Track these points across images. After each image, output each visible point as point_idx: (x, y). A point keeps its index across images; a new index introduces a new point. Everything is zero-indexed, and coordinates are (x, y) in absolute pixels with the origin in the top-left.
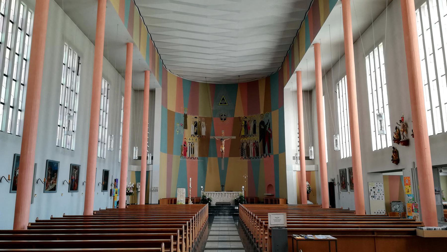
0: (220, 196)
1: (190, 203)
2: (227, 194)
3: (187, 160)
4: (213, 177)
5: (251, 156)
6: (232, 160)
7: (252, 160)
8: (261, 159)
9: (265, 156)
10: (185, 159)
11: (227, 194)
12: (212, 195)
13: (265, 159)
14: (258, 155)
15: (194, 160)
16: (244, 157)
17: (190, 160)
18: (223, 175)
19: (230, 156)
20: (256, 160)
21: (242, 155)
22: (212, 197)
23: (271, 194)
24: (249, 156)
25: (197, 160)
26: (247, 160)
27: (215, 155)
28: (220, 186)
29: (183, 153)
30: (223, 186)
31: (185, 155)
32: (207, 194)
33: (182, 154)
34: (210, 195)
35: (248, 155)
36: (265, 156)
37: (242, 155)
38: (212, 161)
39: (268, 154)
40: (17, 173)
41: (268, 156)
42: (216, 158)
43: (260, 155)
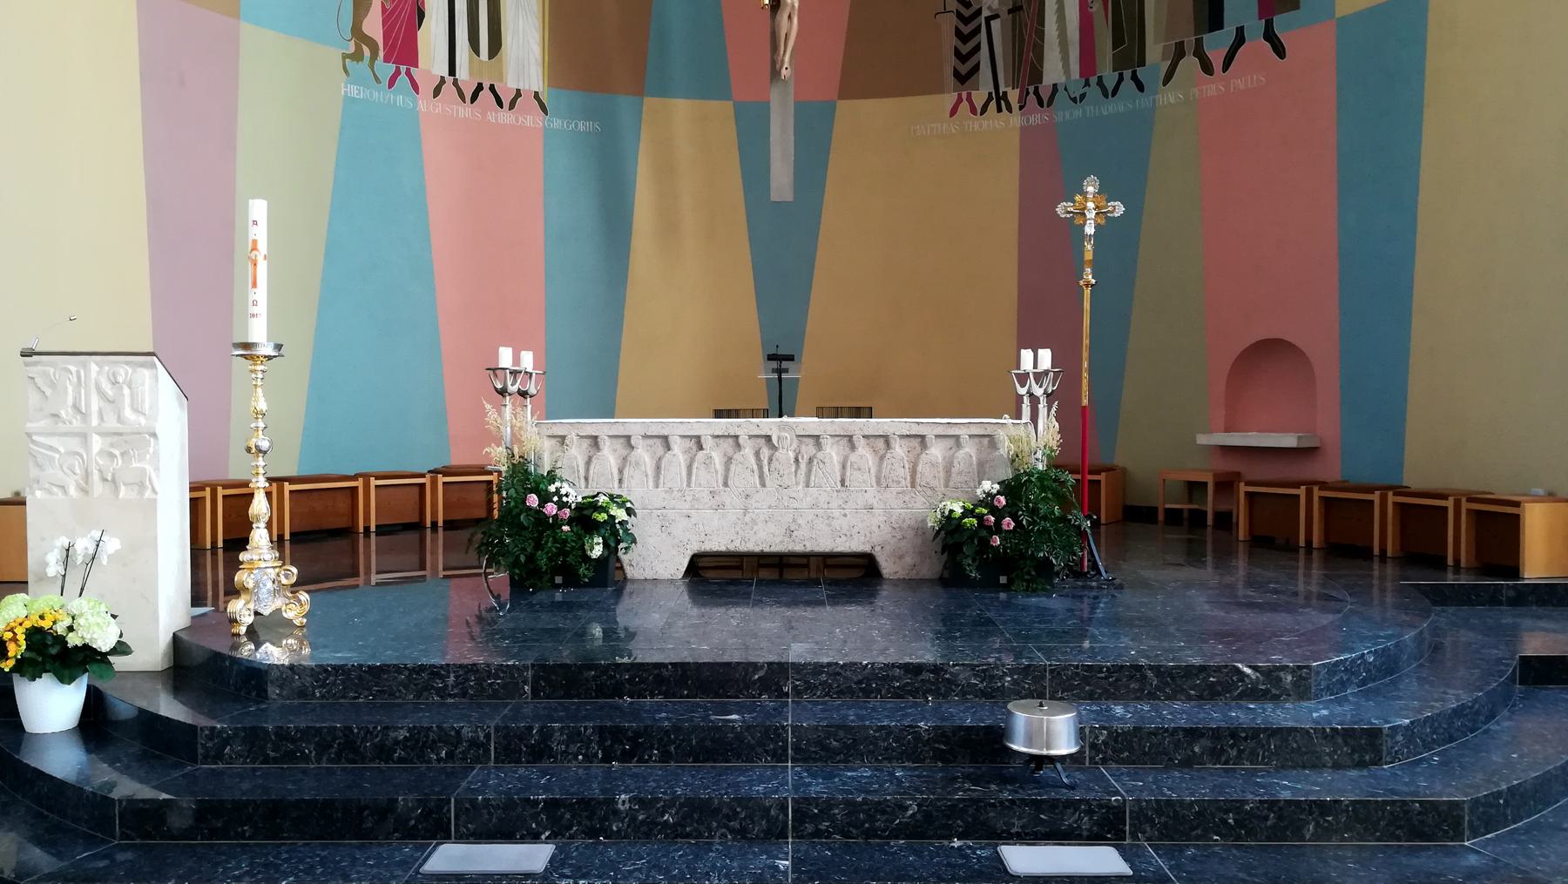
0: (744, 476)
1: (263, 565)
2: (832, 453)
3: (424, 103)
4: (688, 289)
5: (1053, 72)
6: (865, 121)
7: (1064, 113)
8: (1168, 97)
9: (1216, 56)
10: (400, 96)
11: (832, 453)
12: (644, 455)
13: (1213, 87)
14: (1130, 52)
15: (505, 116)
16: (979, 97)
17: (466, 111)
18: (782, 250)
19: (841, 97)
20: (1113, 107)
21: (964, 78)
22: (636, 491)
23: (1289, 441)
24: (1037, 76)
25: (530, 118)
26: (1015, 120)
27: (708, 82)
28: (760, 357)
29: (373, 26)
30: (779, 359)
31: (403, 50)
32: (576, 453)
33: (357, 32)
34: (609, 456)
35: (1028, 68)
36: (1216, 56)
37: (964, 78)
38: (680, 139)
39: (1255, 27)
40: (1541, 492)
41: (1256, 44)
42: (722, 109)
43: (1155, 52)
